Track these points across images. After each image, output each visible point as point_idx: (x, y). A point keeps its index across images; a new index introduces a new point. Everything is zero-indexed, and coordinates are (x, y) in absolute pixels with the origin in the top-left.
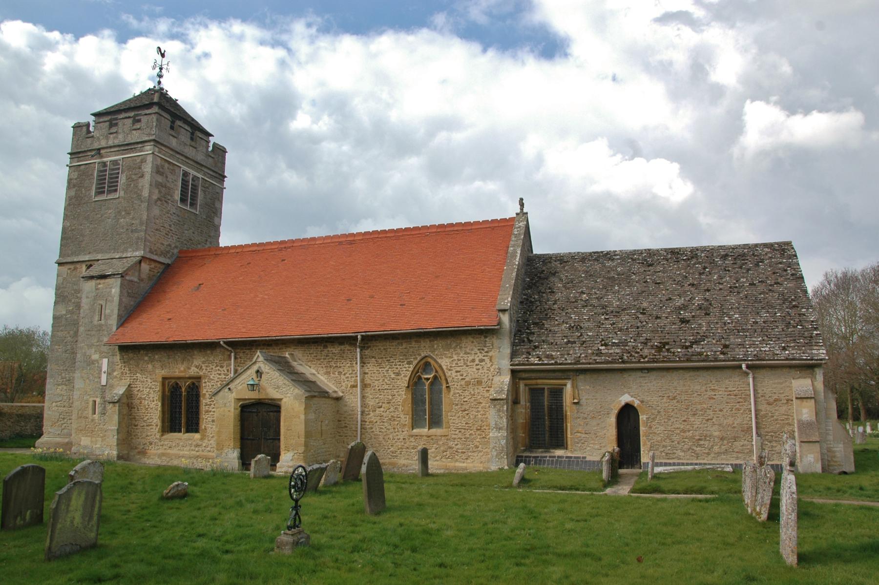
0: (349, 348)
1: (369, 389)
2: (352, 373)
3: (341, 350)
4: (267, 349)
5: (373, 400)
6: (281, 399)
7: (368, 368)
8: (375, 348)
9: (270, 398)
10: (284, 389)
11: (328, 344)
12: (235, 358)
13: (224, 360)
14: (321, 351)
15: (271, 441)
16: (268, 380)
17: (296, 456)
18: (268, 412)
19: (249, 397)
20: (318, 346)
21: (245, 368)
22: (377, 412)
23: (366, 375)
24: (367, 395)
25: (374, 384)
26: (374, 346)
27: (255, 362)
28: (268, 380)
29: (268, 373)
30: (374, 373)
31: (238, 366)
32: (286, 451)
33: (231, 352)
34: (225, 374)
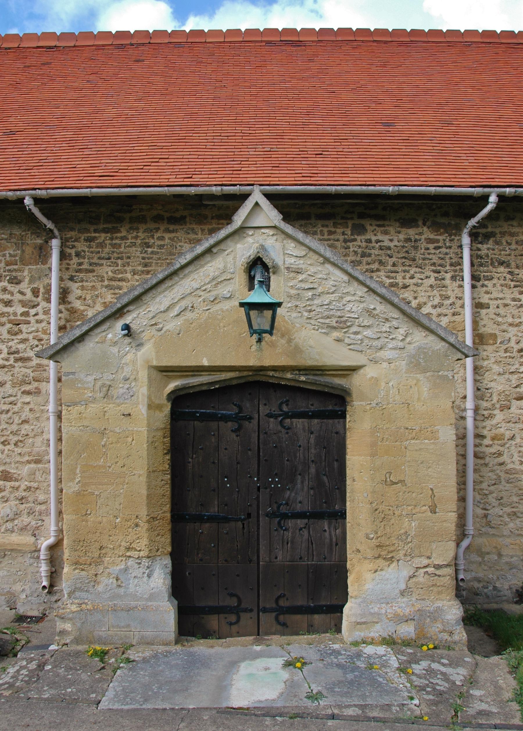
0: (432, 236)
1: (490, 348)
2: (441, 305)
3: (408, 240)
4: (168, 231)
5: (502, 379)
6: (354, 369)
7: (487, 293)
8: (508, 238)
9: (310, 363)
10: (368, 333)
11: (366, 223)
12: (63, 256)
13: (23, 262)
14: (345, 241)
15: (301, 523)
16: (298, 297)
17: (421, 578)
18: (286, 415)
19: (219, 363)
20: (335, 225)
21: (199, 249)
22: (513, 409)
23: (483, 312)
24: (485, 363)
25: (507, 336)
26: (503, 234)
27: (242, 229)
28: (298, 297)
29: (298, 272)
30: (506, 305)
31: (72, 279)
32: (381, 562)
33: (51, 235)
34: (24, 304)
